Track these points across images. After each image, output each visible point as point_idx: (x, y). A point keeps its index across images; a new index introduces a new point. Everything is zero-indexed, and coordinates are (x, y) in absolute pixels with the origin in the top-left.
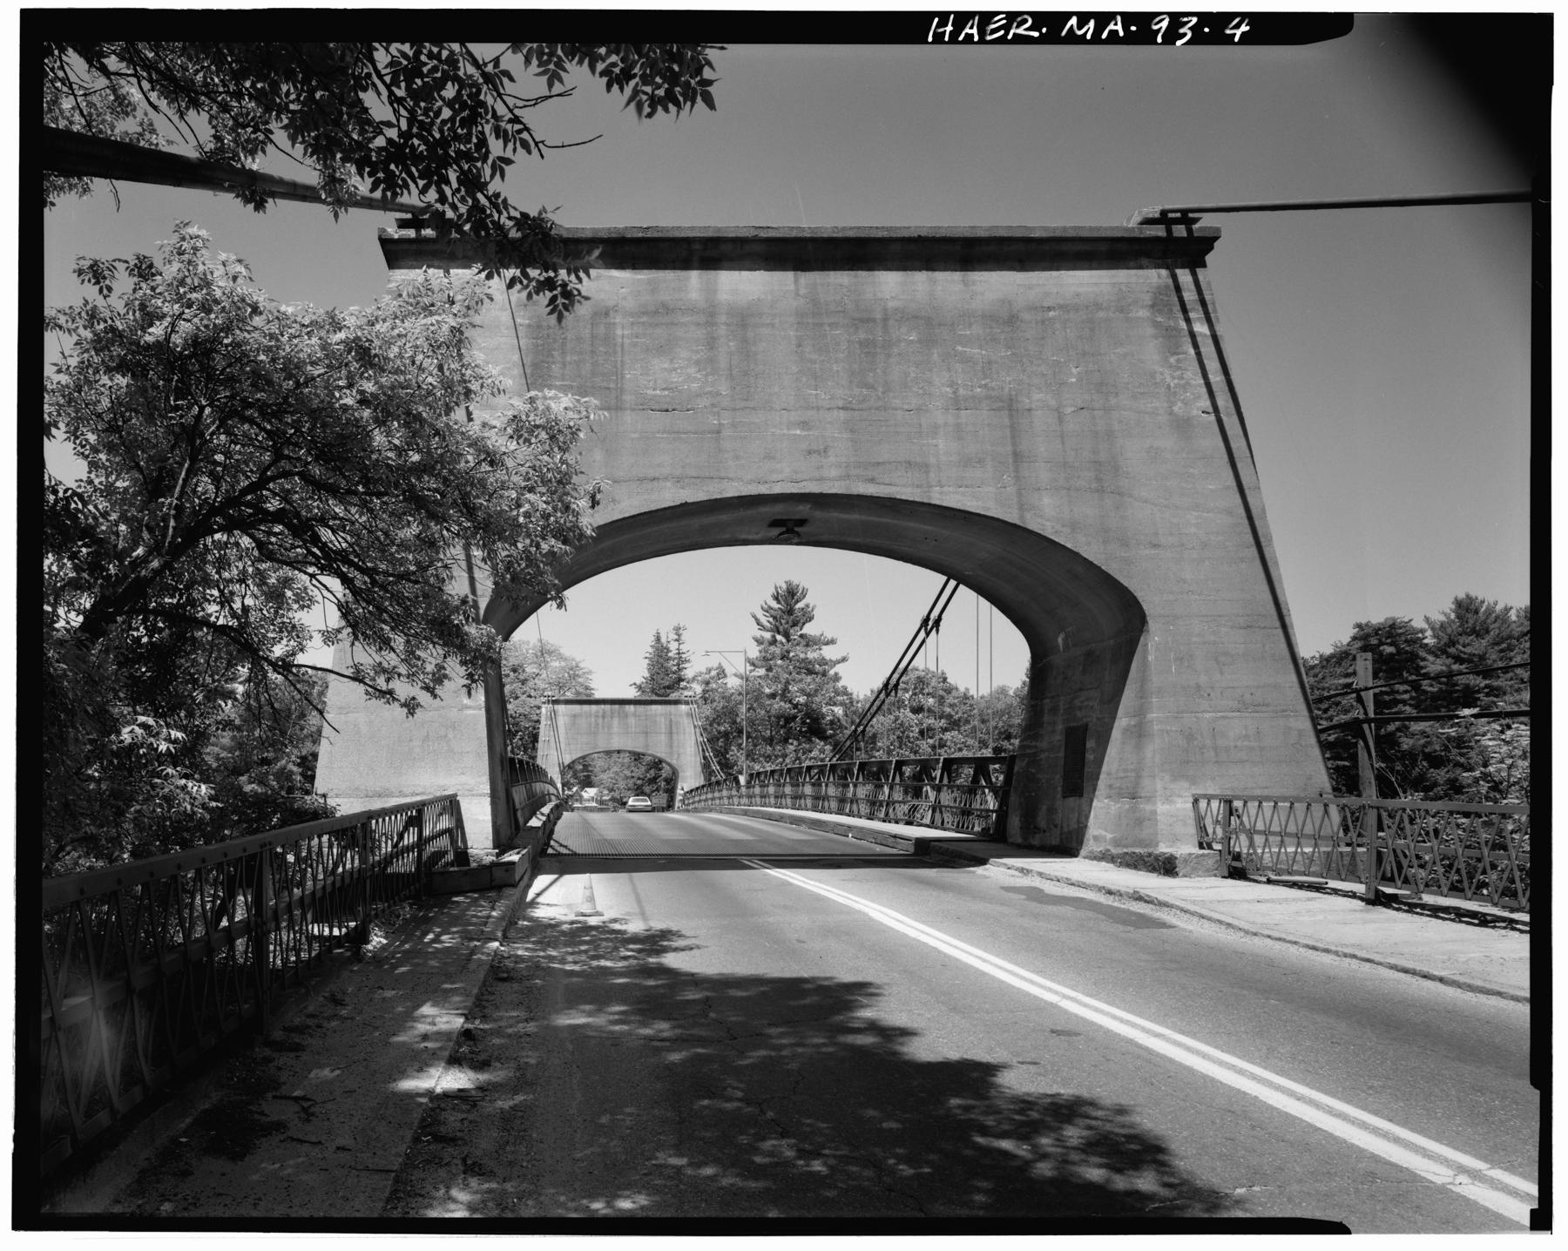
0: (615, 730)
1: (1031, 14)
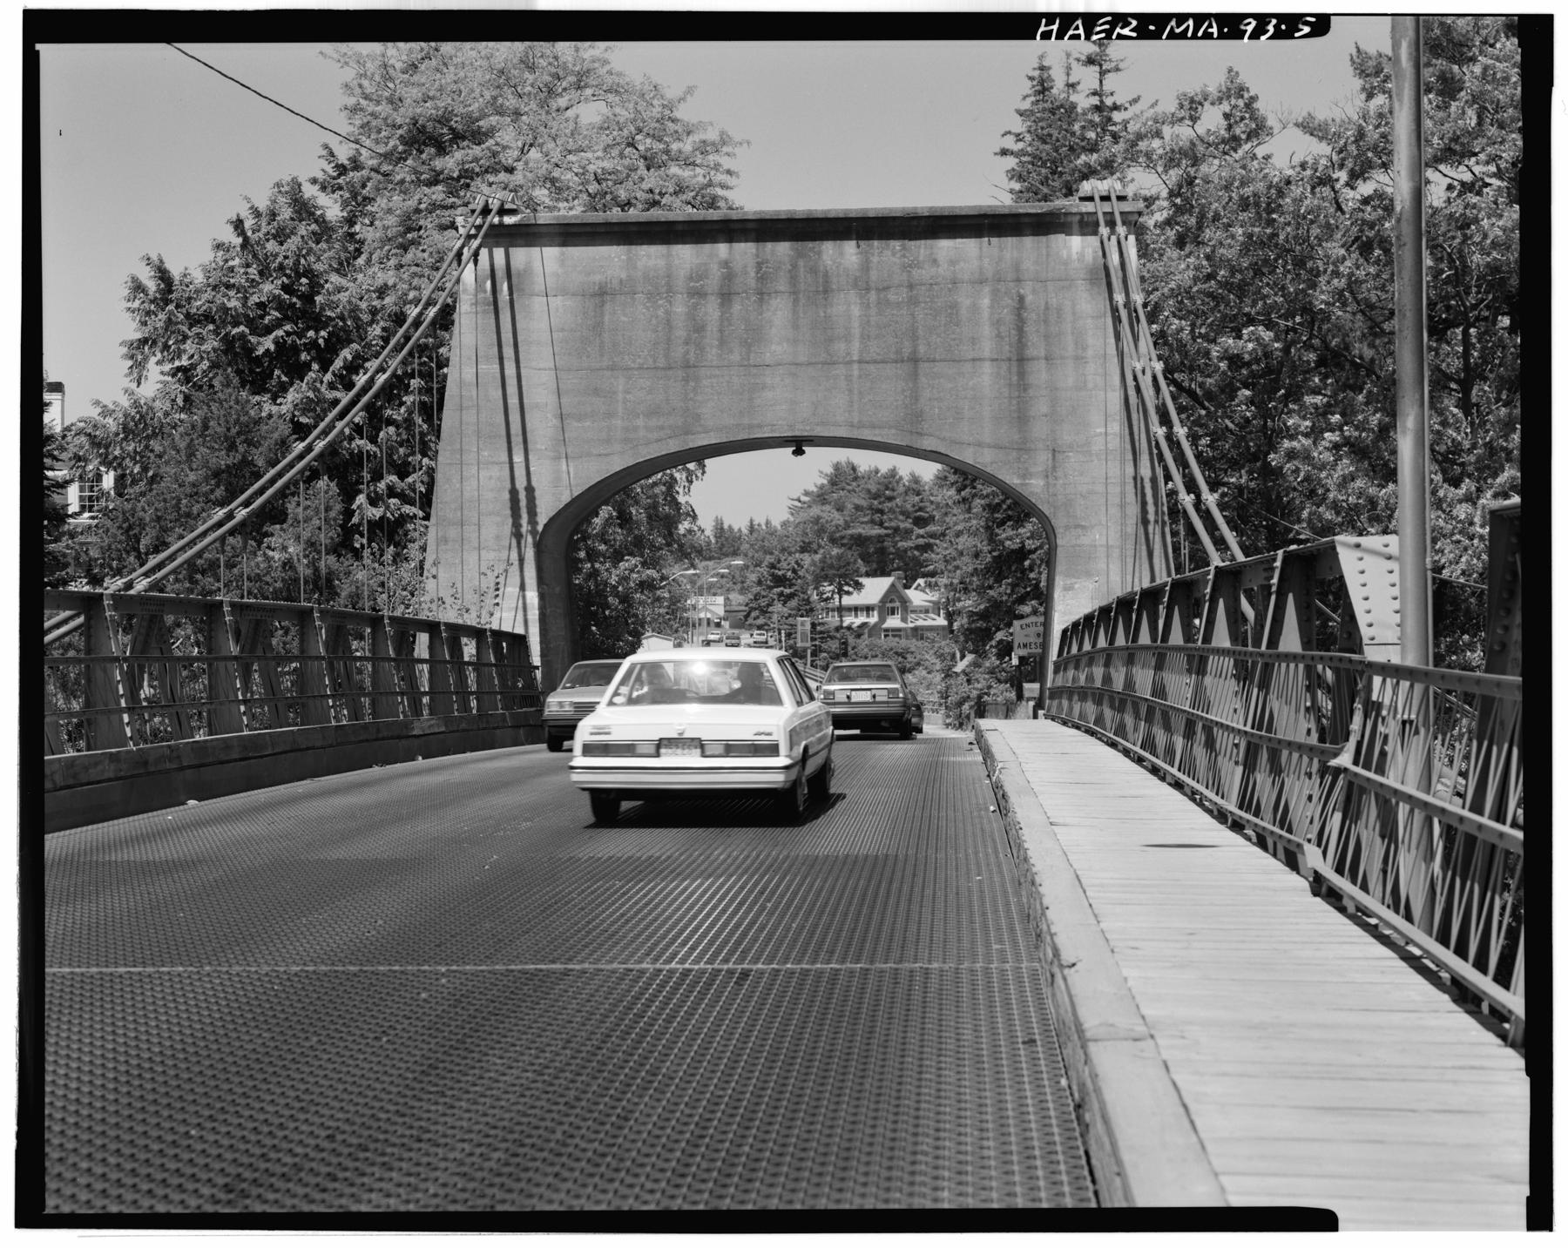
0: (777, 348)
1: (1134, 16)
